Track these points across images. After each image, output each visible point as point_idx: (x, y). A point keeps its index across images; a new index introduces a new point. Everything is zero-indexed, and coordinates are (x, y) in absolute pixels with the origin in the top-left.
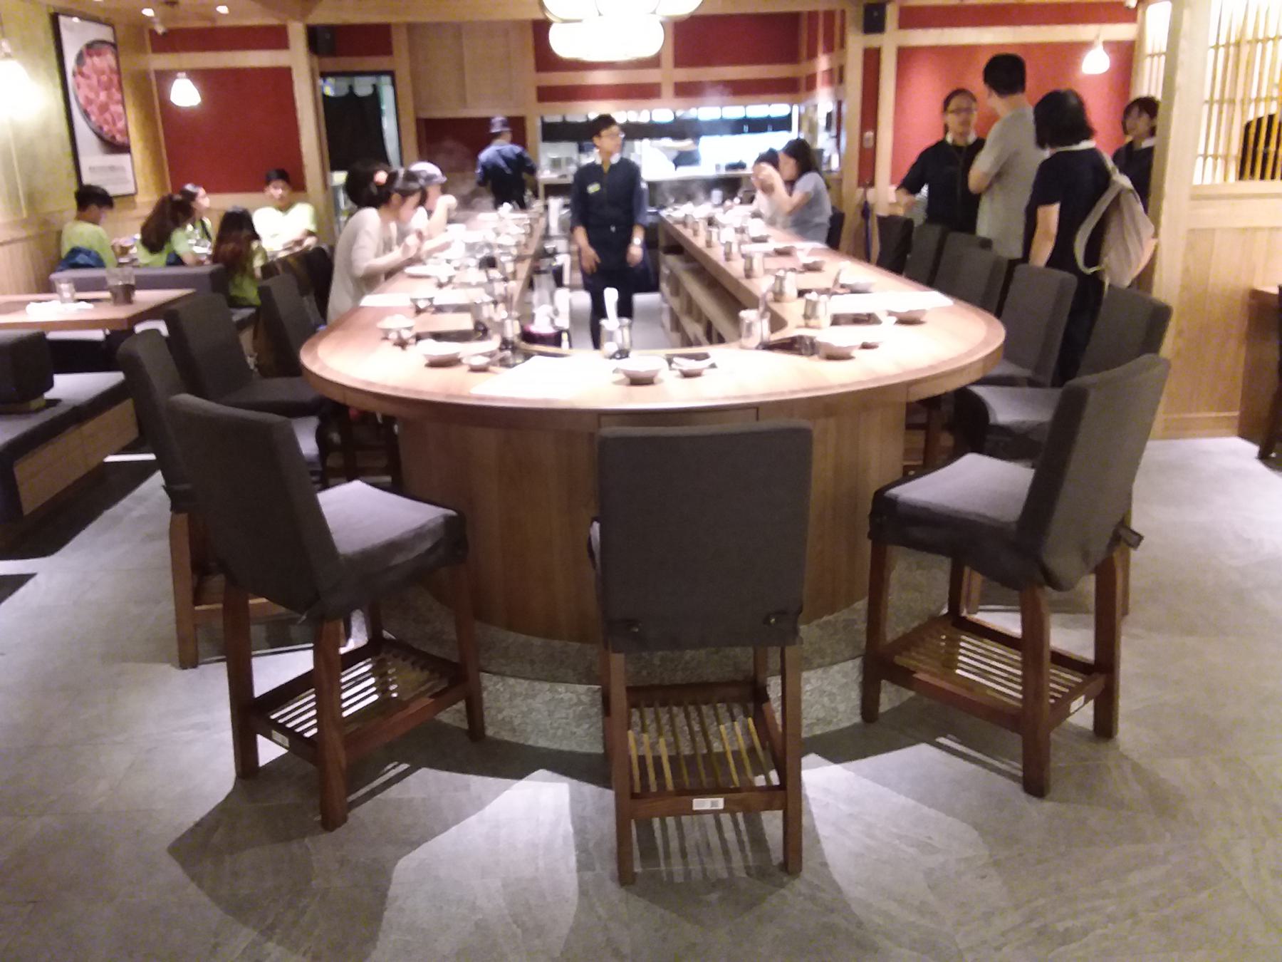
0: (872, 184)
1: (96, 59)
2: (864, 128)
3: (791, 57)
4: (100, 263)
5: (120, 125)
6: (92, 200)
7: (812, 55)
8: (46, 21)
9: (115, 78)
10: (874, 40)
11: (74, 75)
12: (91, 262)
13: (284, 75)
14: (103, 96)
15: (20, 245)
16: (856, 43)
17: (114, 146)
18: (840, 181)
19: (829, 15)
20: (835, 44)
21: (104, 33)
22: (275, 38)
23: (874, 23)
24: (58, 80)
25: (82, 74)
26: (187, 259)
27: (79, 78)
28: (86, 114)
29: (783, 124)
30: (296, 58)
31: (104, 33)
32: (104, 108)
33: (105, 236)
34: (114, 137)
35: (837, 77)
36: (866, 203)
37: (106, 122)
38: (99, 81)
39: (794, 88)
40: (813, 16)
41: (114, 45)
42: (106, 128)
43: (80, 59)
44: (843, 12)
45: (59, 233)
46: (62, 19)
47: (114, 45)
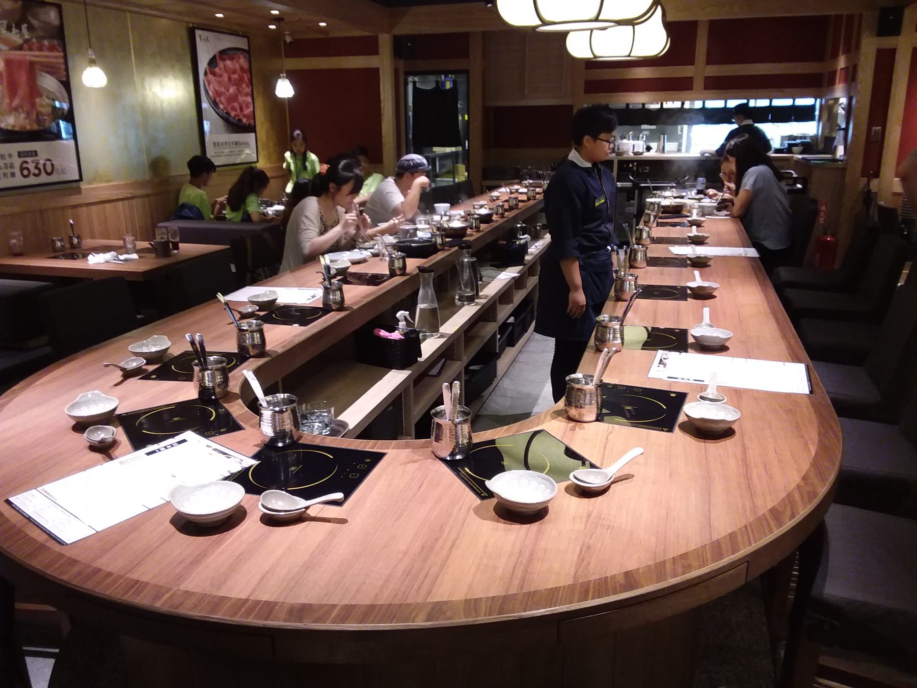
0: (877, 175)
1: (228, 62)
2: (871, 123)
3: (819, 57)
4: (199, 216)
5: (247, 111)
6: (201, 167)
7: (835, 56)
8: (184, 33)
9: (246, 77)
10: (887, 42)
11: (206, 74)
12: (191, 215)
13: (373, 74)
14: (232, 90)
15: (139, 201)
16: (869, 46)
17: (237, 126)
18: (844, 170)
19: (850, 17)
20: (853, 48)
21: (242, 43)
22: (369, 47)
23: (890, 24)
24: (191, 78)
25: (214, 74)
26: (255, 217)
27: (210, 76)
28: (215, 104)
29: (804, 114)
30: (383, 62)
31: (242, 43)
32: (233, 99)
33: (205, 197)
34: (240, 120)
35: (851, 77)
36: (869, 191)
37: (234, 109)
38: (230, 79)
39: (818, 84)
40: (838, 18)
41: (247, 52)
42: (233, 114)
43: (212, 62)
44: (861, 15)
45: (178, 192)
46: (198, 33)
47: (247, 52)
